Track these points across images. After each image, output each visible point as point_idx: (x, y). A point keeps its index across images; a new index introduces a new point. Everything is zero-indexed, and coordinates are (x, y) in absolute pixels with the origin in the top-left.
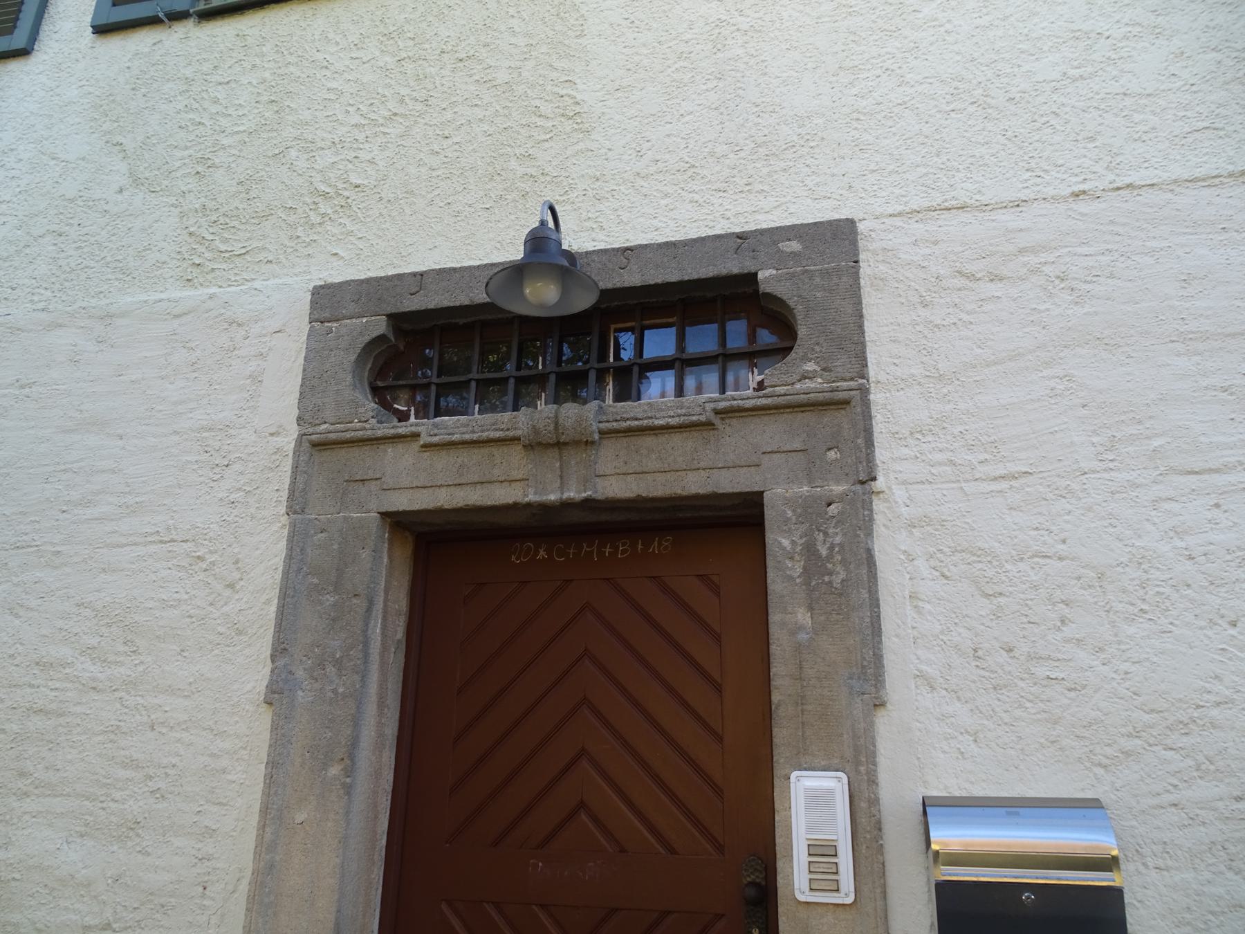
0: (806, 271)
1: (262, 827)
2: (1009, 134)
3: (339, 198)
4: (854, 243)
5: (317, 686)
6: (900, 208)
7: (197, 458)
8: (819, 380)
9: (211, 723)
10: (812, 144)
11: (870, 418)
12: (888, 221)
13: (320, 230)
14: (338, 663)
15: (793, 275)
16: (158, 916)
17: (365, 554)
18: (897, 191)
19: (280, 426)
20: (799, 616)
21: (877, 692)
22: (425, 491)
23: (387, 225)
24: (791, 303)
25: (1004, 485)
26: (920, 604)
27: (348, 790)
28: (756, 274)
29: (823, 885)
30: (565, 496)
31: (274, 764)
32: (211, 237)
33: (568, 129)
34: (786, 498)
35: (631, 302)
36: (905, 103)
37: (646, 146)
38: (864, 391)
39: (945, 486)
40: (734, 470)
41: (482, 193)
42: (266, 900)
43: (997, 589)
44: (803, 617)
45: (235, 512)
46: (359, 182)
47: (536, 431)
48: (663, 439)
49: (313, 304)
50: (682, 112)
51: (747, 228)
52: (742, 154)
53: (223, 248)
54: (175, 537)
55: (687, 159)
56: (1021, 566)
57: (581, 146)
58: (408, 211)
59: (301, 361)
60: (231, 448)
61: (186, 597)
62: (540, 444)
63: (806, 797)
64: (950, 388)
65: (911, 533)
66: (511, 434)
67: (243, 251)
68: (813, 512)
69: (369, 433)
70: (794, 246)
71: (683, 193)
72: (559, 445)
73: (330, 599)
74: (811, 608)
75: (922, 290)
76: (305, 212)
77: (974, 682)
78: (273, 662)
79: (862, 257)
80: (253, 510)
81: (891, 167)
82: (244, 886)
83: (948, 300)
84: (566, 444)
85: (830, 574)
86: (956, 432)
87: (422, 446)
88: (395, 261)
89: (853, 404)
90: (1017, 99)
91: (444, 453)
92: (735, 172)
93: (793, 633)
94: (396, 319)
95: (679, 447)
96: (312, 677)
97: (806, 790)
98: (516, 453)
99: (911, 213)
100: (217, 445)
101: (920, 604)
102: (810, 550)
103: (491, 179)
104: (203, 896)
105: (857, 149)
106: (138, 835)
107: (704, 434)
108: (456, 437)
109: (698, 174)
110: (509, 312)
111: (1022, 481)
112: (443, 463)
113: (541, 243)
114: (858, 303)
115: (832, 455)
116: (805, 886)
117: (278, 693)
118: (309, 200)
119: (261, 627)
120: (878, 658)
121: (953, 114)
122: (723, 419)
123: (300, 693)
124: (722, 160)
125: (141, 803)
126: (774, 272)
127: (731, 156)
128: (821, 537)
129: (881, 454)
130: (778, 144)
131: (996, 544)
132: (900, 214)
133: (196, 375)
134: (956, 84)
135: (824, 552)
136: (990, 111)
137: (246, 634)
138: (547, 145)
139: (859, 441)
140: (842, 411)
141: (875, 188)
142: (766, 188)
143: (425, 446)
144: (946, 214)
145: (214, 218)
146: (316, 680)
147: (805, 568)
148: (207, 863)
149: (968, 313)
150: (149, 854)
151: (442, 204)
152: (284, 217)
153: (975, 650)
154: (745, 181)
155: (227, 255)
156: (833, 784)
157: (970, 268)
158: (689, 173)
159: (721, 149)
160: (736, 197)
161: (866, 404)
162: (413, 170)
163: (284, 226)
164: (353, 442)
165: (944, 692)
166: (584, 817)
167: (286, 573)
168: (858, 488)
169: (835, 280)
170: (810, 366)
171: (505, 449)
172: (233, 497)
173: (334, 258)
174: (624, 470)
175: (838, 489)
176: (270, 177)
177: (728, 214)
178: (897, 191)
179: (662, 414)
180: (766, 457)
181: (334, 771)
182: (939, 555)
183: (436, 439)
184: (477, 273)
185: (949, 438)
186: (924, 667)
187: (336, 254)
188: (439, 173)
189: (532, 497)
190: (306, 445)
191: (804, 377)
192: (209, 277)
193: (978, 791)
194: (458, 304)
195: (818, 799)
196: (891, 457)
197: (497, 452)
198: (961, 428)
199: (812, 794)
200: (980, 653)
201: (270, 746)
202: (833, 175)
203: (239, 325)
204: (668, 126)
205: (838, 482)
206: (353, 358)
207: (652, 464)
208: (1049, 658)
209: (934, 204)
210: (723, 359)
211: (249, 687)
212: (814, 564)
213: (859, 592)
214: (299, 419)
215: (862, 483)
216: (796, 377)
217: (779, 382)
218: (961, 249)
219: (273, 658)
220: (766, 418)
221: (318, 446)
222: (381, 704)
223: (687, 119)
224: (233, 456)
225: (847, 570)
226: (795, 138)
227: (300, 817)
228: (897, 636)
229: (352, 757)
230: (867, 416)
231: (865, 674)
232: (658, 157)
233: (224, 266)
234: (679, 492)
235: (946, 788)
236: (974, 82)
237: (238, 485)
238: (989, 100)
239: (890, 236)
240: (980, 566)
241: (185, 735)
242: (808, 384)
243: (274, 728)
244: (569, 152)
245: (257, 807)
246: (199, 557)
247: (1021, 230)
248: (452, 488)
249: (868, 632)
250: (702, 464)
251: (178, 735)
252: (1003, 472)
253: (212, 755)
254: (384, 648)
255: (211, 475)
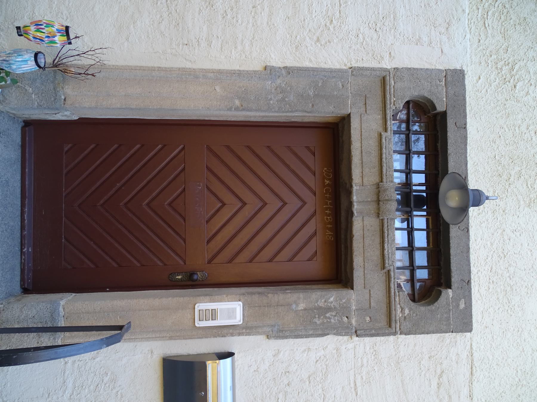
0: (450, 310)
1: (213, 71)
2: (503, 394)
3: (509, 77)
4: (461, 331)
5: (273, 91)
6: (474, 348)
7: (380, 12)
8: (400, 315)
9: (256, 38)
10: (509, 311)
11: (383, 336)
12: (469, 344)
13: (494, 68)
14: (283, 99)
15: (449, 305)
16: (174, 22)
17: (331, 108)
18: (482, 347)
19: (394, 57)
20: (302, 305)
21: (273, 337)
22: (360, 135)
23: (492, 105)
24: (436, 304)
25: (352, 385)
26: (306, 352)
27: (230, 109)
28: (451, 288)
29: (201, 315)
30: (355, 204)
31: (239, 74)
32: (496, 5)
33: (532, 196)
34: (350, 299)
35: (441, 228)
36: (524, 351)
37: (518, 234)
38: (395, 334)
39: (353, 363)
40: (363, 278)
41: (503, 154)
42: (183, 77)
43: (312, 381)
44: (302, 306)
45: (353, 38)
46: (517, 87)
47: (385, 190)
48: (378, 246)
49: (455, 71)
50: (533, 251)
51: (473, 284)
52: (508, 279)
53: (490, 14)
54: (342, 7)
55: (509, 254)
56: (320, 390)
57: (522, 202)
58: (498, 116)
59: (427, 66)
60: (385, 31)
61: (314, 17)
62: (379, 192)
63: (233, 308)
64: (393, 366)
65: (334, 349)
66: (384, 177)
67: (487, 25)
68: (344, 310)
69: (389, 107)
70: (462, 306)
71: (492, 252)
72: (378, 201)
73: (311, 93)
74: (305, 309)
75: (437, 357)
76: (505, 58)
77: (277, 371)
78: (284, 68)
79: (454, 334)
80: (354, 47)
81: (494, 344)
82: (189, 65)
83: (431, 367)
84: (379, 204)
85: (319, 317)
86: (375, 368)
87: (380, 133)
88: (473, 111)
89: (390, 329)
90: (519, 398)
91: (377, 144)
92: (500, 276)
93: (295, 302)
94: (444, 114)
95: (374, 254)
96: (277, 87)
97: (236, 308)
98: (375, 179)
99: (472, 353)
100: (386, 24)
101: (306, 352)
102: (329, 309)
103: (510, 158)
104: (183, 44)
105: (504, 330)
106: (207, 7)
107: (380, 265)
108: (384, 150)
109: (501, 259)
110: (443, 178)
111: (354, 392)
112: (371, 144)
113: (478, 199)
114: (433, 333)
115: (368, 319)
116: (201, 308)
117: (269, 71)
118: (510, 60)
119: (299, 59)
120: (286, 337)
121: (515, 372)
122: (386, 273)
123: (270, 82)
124: (507, 270)
125: (221, 6)
126: (451, 297)
127: (508, 275)
128: (334, 314)
129: (367, 339)
130: (511, 296)
131: (329, 382)
132: (471, 348)
133: (423, 6)
134: (530, 373)
135: (328, 315)
136: (515, 387)
137: (296, 51)
138: (525, 185)
139: (373, 331)
140: (387, 324)
141: (485, 338)
142: (490, 290)
143: (380, 135)
144: (469, 367)
145: (507, 6)
146: (276, 90)
147: (321, 307)
148: (197, 44)
149: (425, 375)
150: (199, 14)
151: (500, 133)
152: (503, 47)
153: (288, 372)
154: (495, 280)
155: (485, 16)
156: (238, 319)
157: (444, 377)
158: (502, 255)
159: (512, 269)
160: (488, 277)
161: (389, 334)
162: (520, 116)
163: (498, 47)
164: (384, 98)
165: (272, 360)
166: (220, 204)
167: (324, 70)
168: (354, 331)
169: (445, 323)
170: (407, 311)
171: (377, 174)
172: (360, 36)
173: (477, 77)
174: (365, 229)
175: (354, 322)
176: (526, 36)
177: (480, 273)
178: (482, 347)
179: (390, 248)
180: (368, 291)
181: (237, 102)
182: (325, 360)
183: (384, 140)
184: (463, 157)
185: (373, 365)
186: (282, 353)
187: (480, 78)
188: (517, 131)
189: (355, 188)
190: (384, 74)
191: (402, 309)
192: (474, 7)
193: (237, 371)
194: (449, 147)
195: (231, 313)
196: (365, 344)
197: (376, 170)
198: (376, 370)
199: (234, 310)
200: (287, 374)
201: (247, 71)
202: (493, 320)
203: (447, 28)
204: (527, 245)
205: (356, 321)
206: (426, 95)
207: (367, 242)
208: (286, 399)
209: (475, 363)
210: (412, 267)
211: (273, 56)
212: (323, 311)
213: (312, 329)
214: (397, 69)
215: (356, 332)
216: (402, 305)
217: (401, 298)
218: (453, 373)
219: (285, 68)
220: (385, 292)
221: (384, 80)
222: (263, 117)
223: (529, 253)
224: (380, 33)
225: (321, 324)
226: (513, 303)
227: (217, 88)
228: (294, 343)
229: (243, 110)
230: (384, 335)
231: (280, 332)
232: (511, 240)
233: (480, 15)
234: (355, 254)
235: (238, 360)
236: (530, 381)
237: (366, 38)
238: (520, 387)
239: (462, 344)
240: (321, 375)
241: (251, 25)
242: (399, 310)
243: (255, 72)
244: (520, 197)
245: (222, 67)
246: (332, 21)
247: (459, 397)
248: (360, 149)
249: (296, 334)
250: (366, 264)
251: (251, 21)
252: (358, 385)
253: (242, 41)
254: (287, 116)
255: (372, 22)
